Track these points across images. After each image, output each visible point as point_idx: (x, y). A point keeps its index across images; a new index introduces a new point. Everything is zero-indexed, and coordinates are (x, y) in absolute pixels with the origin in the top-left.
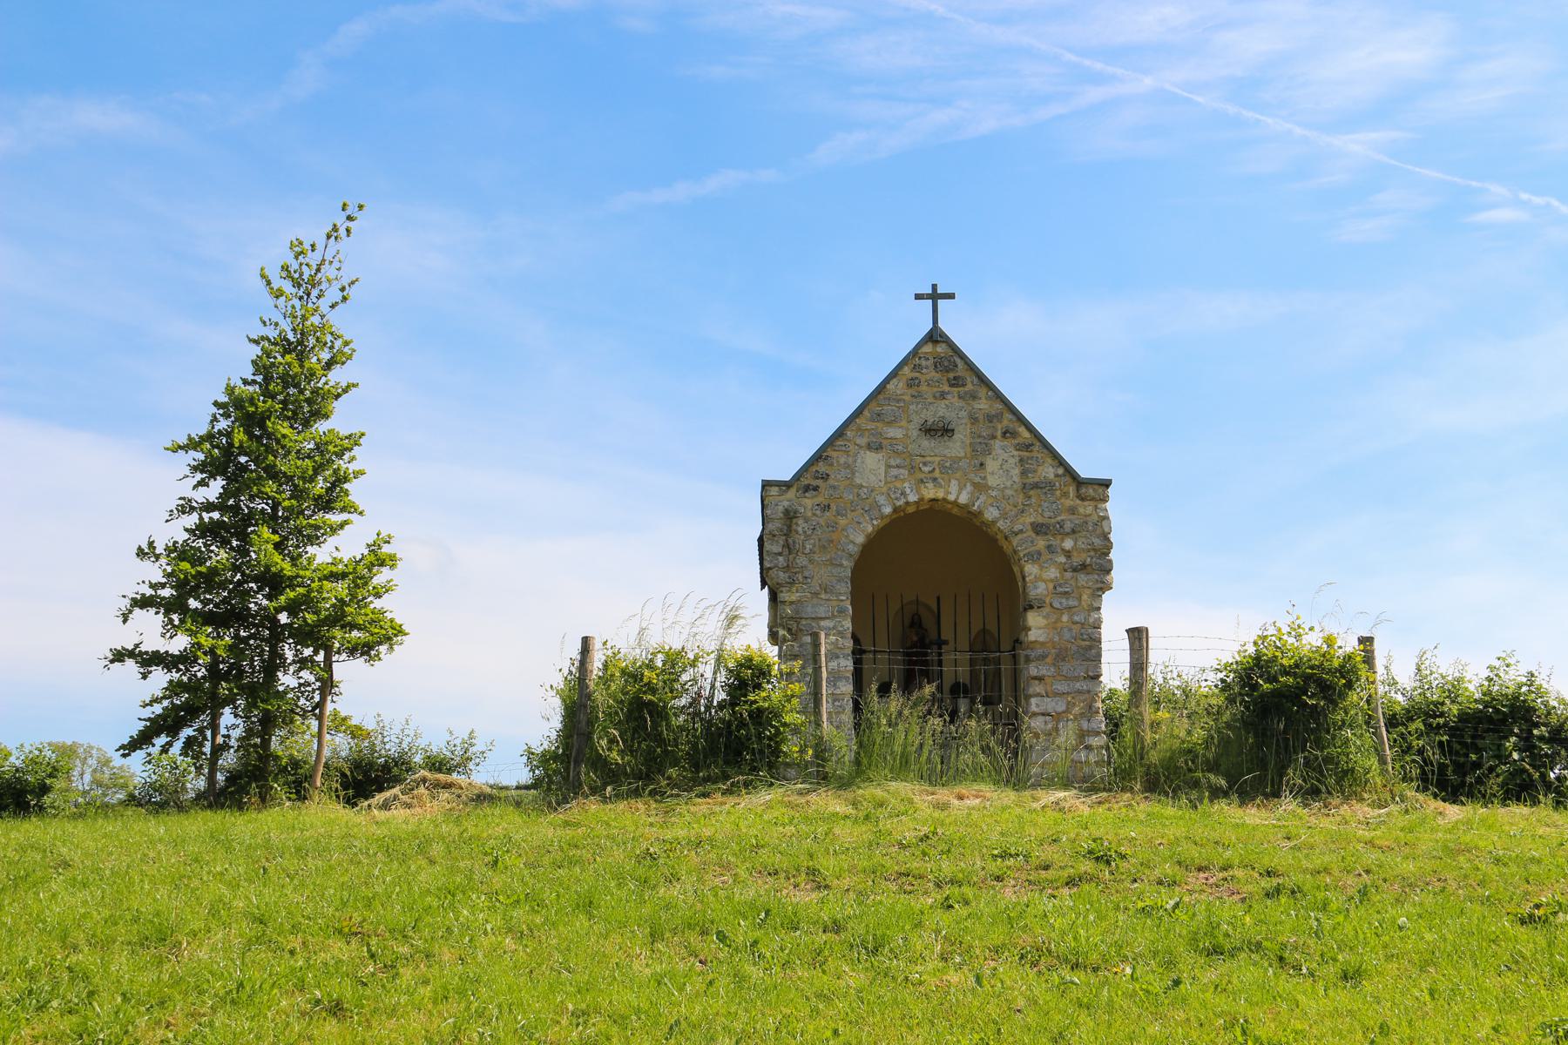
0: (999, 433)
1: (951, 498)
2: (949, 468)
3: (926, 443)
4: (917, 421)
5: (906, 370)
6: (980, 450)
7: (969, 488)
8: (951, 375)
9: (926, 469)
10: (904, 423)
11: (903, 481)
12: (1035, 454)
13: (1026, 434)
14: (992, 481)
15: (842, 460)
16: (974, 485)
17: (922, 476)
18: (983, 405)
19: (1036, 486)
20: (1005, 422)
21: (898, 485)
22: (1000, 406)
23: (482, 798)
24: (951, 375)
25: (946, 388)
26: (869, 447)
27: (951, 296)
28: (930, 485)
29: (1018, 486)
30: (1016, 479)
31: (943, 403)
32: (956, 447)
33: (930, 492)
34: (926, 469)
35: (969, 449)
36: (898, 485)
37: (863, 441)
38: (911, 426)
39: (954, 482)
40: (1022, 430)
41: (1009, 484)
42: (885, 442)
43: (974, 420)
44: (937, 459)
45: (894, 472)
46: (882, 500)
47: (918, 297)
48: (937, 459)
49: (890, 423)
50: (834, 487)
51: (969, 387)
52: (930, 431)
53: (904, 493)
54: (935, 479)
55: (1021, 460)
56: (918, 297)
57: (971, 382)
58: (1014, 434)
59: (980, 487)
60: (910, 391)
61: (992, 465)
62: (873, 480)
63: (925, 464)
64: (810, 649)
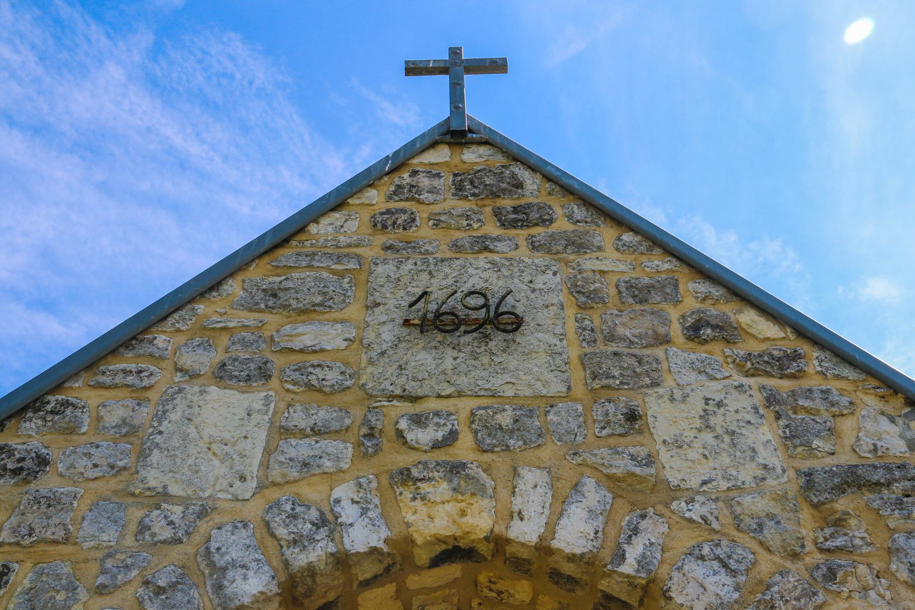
0: (676, 331)
1: (526, 532)
2: (508, 434)
3: (426, 359)
4: (395, 301)
5: (373, 196)
6: (617, 387)
7: (594, 494)
8: (507, 203)
9: (423, 436)
10: (354, 311)
11: (333, 477)
12: (815, 383)
13: (770, 330)
14: (676, 469)
15: (115, 414)
16: (616, 484)
17: (404, 459)
18: (610, 259)
19: (852, 480)
20: (690, 304)
21: (312, 492)
22: (666, 265)
23: (403, 416)
24: (507, 203)
25: (492, 229)
26: (222, 374)
27: (497, 66)
28: (440, 489)
29: (790, 483)
30: (775, 460)
31: (482, 260)
32: (534, 367)
33: (436, 515)
34: (423, 436)
35: (578, 375)
36: (312, 492)
37: (203, 360)
38: (380, 315)
39: (529, 476)
40: (748, 318)
41: (747, 474)
42: (278, 362)
43: (585, 296)
44: (466, 405)
45: (301, 449)
46: (234, 545)
47: (413, 69)
48: (466, 405)
49: (306, 312)
50: (52, 502)
51: (562, 225)
52: (437, 322)
53: (328, 522)
54: (455, 469)
55: (771, 399)
56: (413, 69)
57: (564, 218)
58: (727, 333)
59: (640, 492)
60: (381, 239)
61: (665, 417)
62: (214, 479)
63: (418, 421)
64: (423, 300)
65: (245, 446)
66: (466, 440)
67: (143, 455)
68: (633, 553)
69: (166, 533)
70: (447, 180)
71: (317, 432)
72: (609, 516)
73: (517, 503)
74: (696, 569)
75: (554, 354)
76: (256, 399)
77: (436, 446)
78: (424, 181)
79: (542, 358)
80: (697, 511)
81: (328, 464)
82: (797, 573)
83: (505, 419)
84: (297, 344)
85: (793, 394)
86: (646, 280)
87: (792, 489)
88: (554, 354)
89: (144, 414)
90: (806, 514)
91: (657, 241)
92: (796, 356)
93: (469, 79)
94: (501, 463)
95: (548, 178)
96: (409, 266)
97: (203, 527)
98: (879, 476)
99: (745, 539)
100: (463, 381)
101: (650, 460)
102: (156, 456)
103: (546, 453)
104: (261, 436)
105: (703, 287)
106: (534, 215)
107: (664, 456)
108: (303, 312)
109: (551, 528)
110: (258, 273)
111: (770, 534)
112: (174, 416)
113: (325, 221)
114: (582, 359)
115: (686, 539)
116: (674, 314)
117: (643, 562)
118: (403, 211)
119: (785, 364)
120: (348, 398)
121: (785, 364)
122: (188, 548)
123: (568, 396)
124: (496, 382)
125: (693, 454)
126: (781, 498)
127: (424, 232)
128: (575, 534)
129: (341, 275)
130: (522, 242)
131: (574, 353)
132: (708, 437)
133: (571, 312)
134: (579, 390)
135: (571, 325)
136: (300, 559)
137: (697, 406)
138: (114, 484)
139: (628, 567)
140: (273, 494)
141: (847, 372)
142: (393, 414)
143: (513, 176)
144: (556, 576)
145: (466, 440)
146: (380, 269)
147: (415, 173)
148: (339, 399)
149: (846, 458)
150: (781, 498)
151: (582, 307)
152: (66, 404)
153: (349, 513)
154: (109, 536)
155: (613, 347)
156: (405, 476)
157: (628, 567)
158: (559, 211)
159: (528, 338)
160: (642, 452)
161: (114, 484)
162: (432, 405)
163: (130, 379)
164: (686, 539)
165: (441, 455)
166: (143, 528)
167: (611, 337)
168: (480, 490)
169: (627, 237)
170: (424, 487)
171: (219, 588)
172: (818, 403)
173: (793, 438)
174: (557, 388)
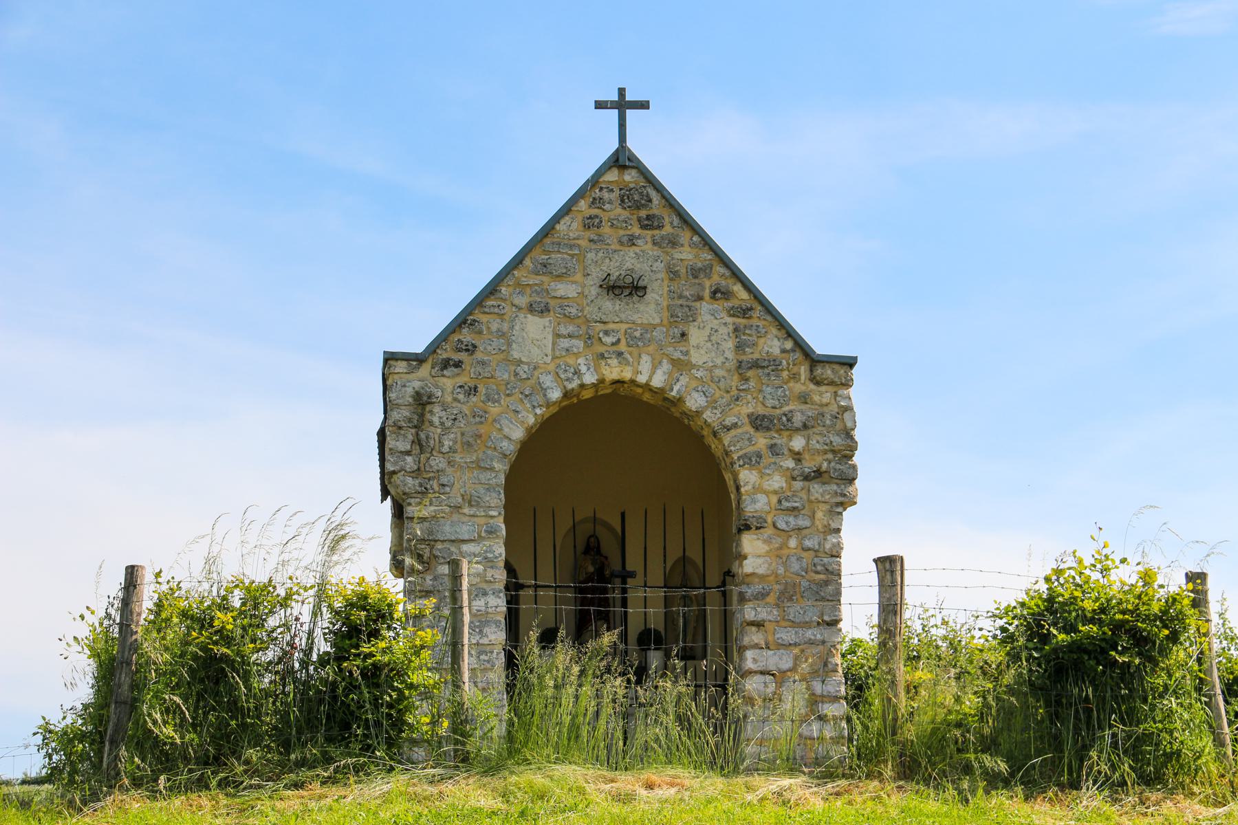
0: (707, 294)
1: (642, 379)
2: (638, 339)
3: (609, 305)
4: (597, 274)
7: (666, 366)
8: (643, 213)
9: (608, 340)
10: (578, 277)
11: (577, 355)
12: (755, 322)
13: (744, 295)
14: (696, 357)
16: (675, 363)
17: (601, 349)
19: (756, 365)
20: (716, 278)
21: (571, 361)
22: (708, 256)
24: (643, 213)
25: (637, 231)
26: (531, 309)
27: (644, 105)
28: (614, 362)
29: (732, 364)
30: (730, 355)
32: (649, 311)
33: (613, 371)
34: (608, 340)
35: (666, 314)
36: (571, 361)
37: (522, 301)
38: (589, 281)
40: (737, 288)
41: (719, 361)
42: (552, 303)
43: (673, 274)
44: (624, 327)
45: (565, 343)
46: (548, 380)
47: (600, 105)
48: (624, 327)
50: (483, 363)
51: (668, 229)
53: (577, 373)
56: (600, 105)
57: (669, 220)
58: (727, 295)
59: (681, 365)
61: (696, 336)
62: (536, 355)
63: (606, 333)
65: (545, 341)
66: (623, 341)
67: (509, 345)
68: (676, 388)
69: (525, 376)
70: (615, 195)
71: (570, 336)
72: (670, 374)
73: (640, 368)
74: (695, 395)
75: (658, 304)
76: (545, 321)
77: (613, 344)
78: (606, 195)
79: (653, 306)
80: (699, 374)
81: (575, 350)
82: (727, 396)
83: (637, 334)
84: (558, 294)
85: (745, 327)
86: (700, 265)
87: (733, 368)
88: (658, 304)
89: (505, 326)
90: (736, 377)
91: (707, 243)
92: (751, 309)
93: (630, 113)
94: (635, 351)
95: (663, 197)
96: (600, 254)
97: (536, 373)
98: (765, 364)
99: (713, 385)
100: (623, 316)
101: (687, 353)
102: (514, 346)
103: (651, 349)
104: (550, 337)
105: (722, 270)
106: (656, 224)
107: (692, 352)
108: (558, 276)
109: (651, 377)
110: (538, 255)
111: (722, 385)
112: (517, 328)
113: (562, 222)
114: (668, 306)
115: (694, 384)
116: (707, 283)
117: (678, 392)
118: (597, 216)
119: (745, 312)
120: (580, 321)
121: (745, 312)
122: (532, 381)
123: (661, 324)
124: (635, 317)
125: (703, 352)
126: (729, 371)
127: (606, 229)
128: (658, 381)
129: (572, 256)
130: (649, 240)
131: (665, 304)
132: (709, 344)
133: (666, 282)
134: (665, 322)
135: (666, 289)
136: (570, 386)
137: (707, 331)
138: (502, 356)
139: (674, 393)
140: (557, 361)
141: (769, 318)
142: (597, 330)
143: (648, 195)
144: (651, 390)
145: (623, 341)
146: (589, 255)
147: (601, 189)
148: (577, 321)
149: (756, 356)
150: (729, 371)
151: (671, 279)
152: (474, 321)
153: (583, 369)
154: (506, 376)
155: (680, 302)
156: (602, 356)
157: (674, 393)
158: (667, 219)
159: (650, 296)
160: (685, 349)
161: (502, 356)
162: (611, 326)
163: (496, 310)
164: (694, 384)
165: (615, 348)
166: (516, 374)
167: (680, 297)
168: (628, 363)
169: (696, 238)
170: (609, 361)
171: (545, 395)
172: (753, 332)
173: (739, 348)
174: (657, 321)
